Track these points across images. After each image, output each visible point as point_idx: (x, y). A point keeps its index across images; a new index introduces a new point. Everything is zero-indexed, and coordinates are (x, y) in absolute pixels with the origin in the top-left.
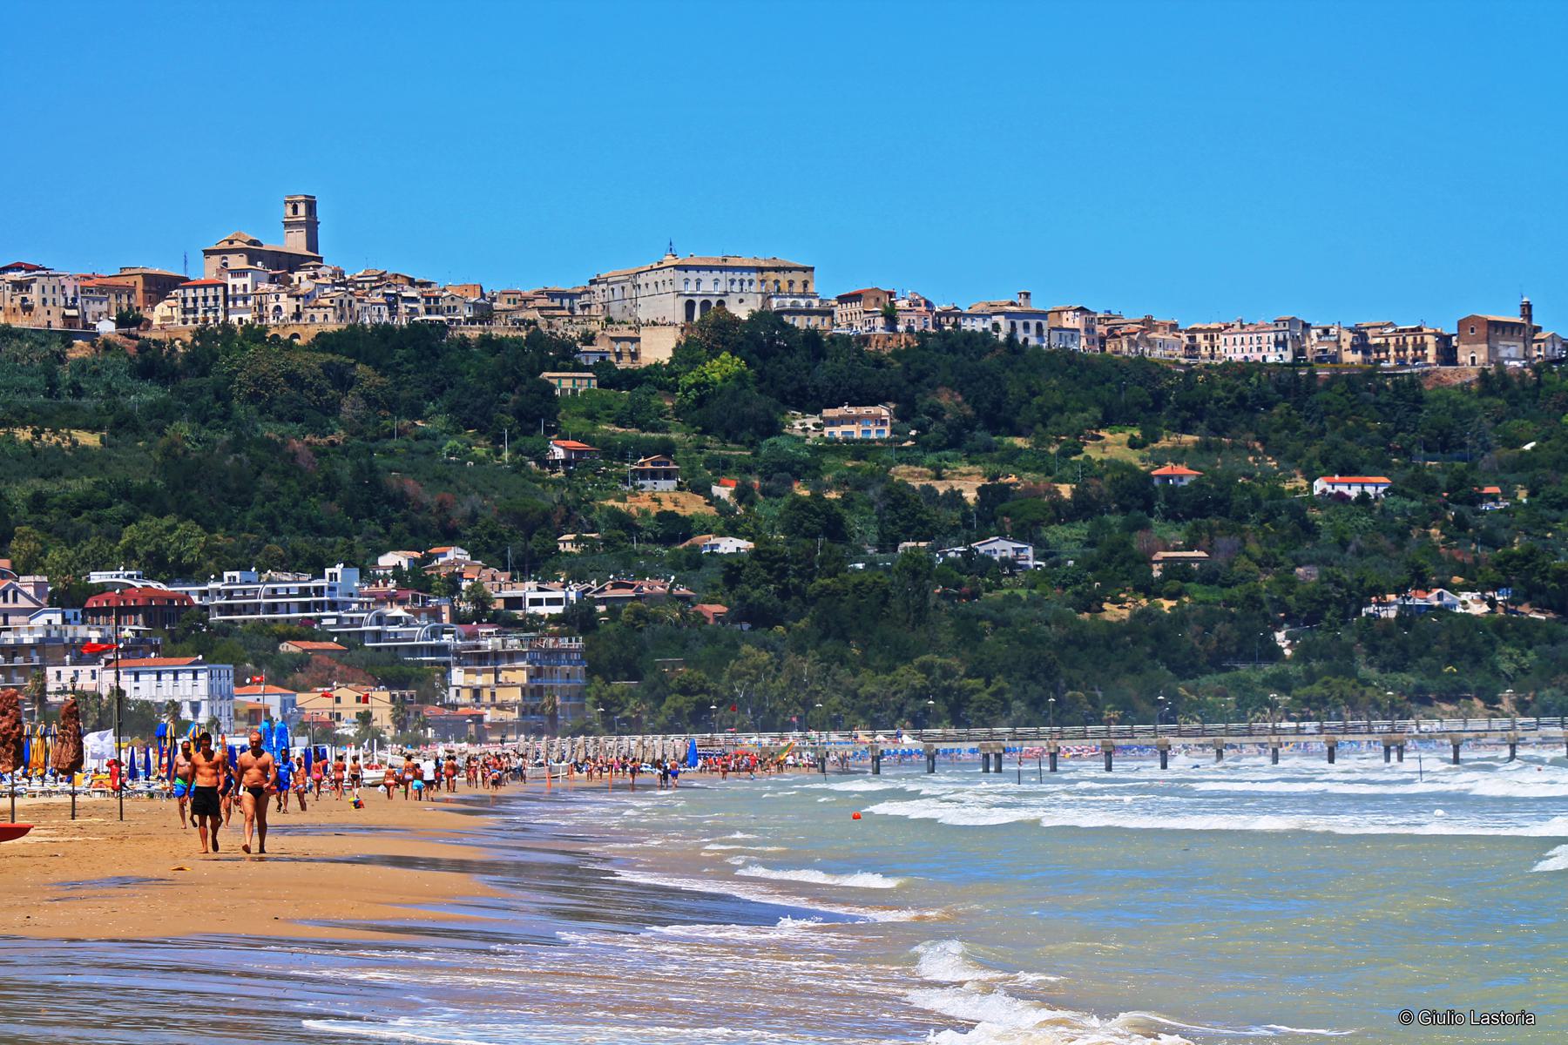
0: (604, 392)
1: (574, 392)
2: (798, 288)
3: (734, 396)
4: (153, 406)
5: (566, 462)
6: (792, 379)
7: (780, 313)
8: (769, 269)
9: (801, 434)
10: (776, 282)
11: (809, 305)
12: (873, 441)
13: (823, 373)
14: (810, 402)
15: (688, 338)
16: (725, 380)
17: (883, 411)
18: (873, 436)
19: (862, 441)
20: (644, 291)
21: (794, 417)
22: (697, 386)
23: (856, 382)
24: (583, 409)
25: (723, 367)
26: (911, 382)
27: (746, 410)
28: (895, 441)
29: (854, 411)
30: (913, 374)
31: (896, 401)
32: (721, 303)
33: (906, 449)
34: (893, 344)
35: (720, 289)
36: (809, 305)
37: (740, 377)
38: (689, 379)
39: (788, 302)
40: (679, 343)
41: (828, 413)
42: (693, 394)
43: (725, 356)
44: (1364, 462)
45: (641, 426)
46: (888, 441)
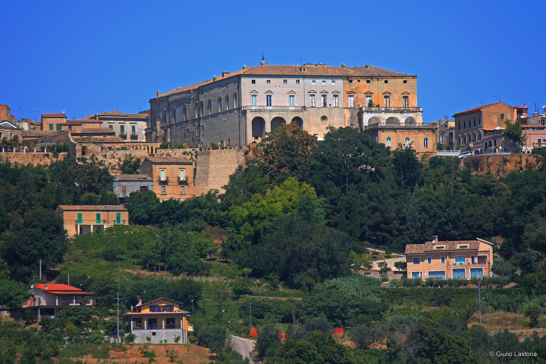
0: (138, 228)
1: (98, 228)
2: (396, 102)
3: (290, 228)
4: (196, 275)
5: (47, 311)
6: (374, 210)
7: (374, 130)
8: (359, 78)
9: (378, 276)
10: (369, 94)
11: (411, 121)
12: (465, 283)
13: (413, 201)
14: (390, 235)
15: (248, 162)
16: (286, 210)
17: (484, 246)
18: (468, 276)
19: (450, 283)
20: (206, 112)
21: (375, 257)
22: (251, 218)
23: (453, 213)
24: (101, 250)
25: (286, 195)
26: (521, 210)
27: (305, 245)
28: (494, 281)
29: (445, 246)
30: (523, 199)
31: (505, 235)
32: (298, 121)
33: (507, 292)
34: (510, 167)
35: (298, 102)
36: (411, 121)
37: (305, 209)
38: (241, 212)
39: (384, 117)
40: (240, 168)
41: (412, 249)
42: (248, 229)
43: (291, 181)
44: (329, 273)
45: (172, 269)
46: (485, 282)
